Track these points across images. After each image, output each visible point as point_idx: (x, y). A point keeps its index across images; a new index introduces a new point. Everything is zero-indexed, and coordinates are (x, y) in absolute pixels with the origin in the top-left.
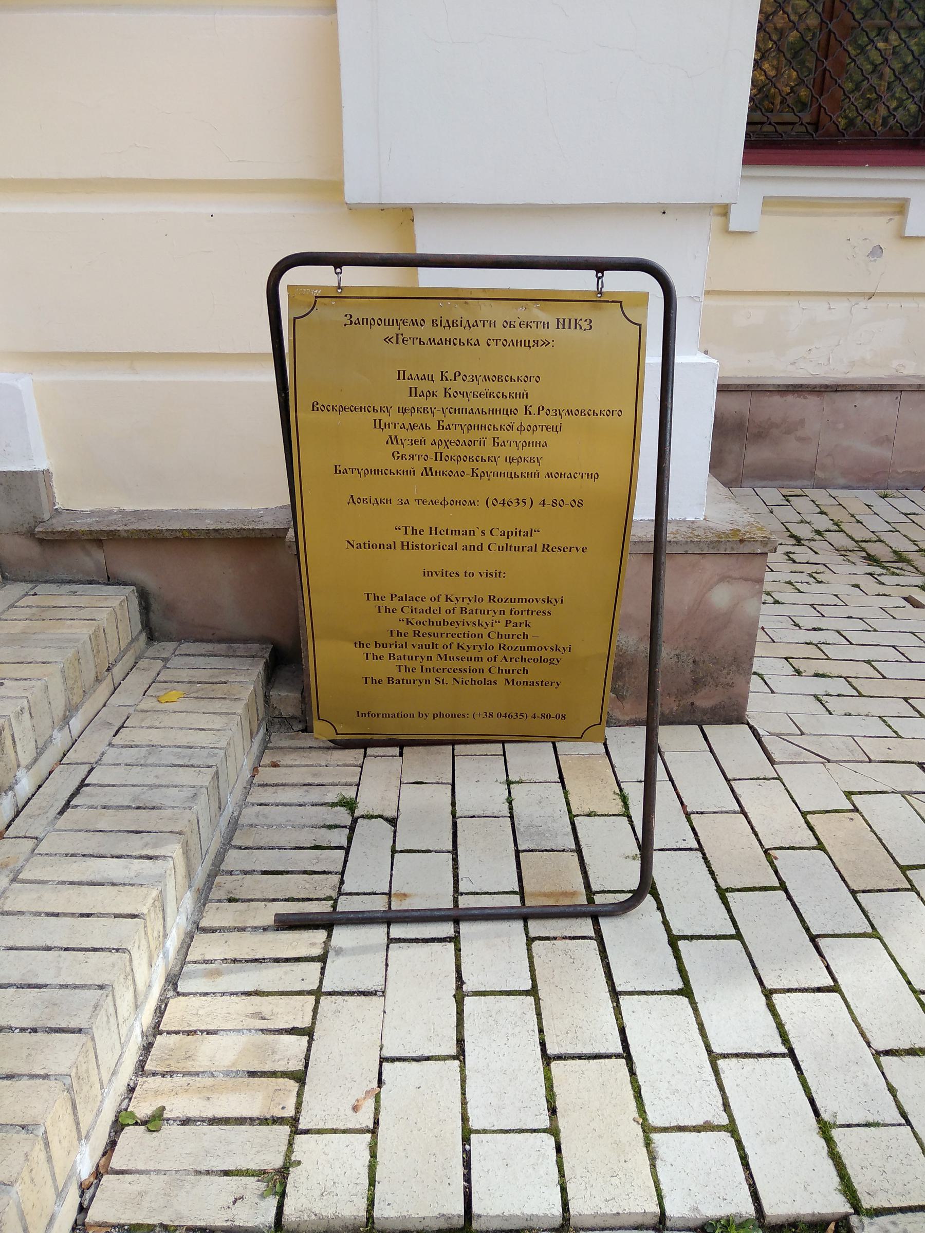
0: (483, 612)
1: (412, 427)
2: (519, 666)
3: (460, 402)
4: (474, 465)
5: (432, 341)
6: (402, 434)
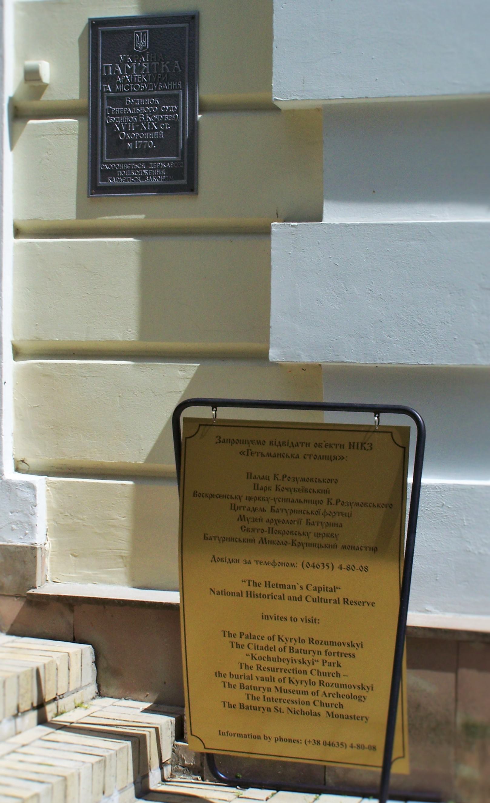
0: (305, 652)
1: (255, 510)
2: (336, 701)
3: (286, 494)
4: (294, 537)
5: (269, 455)
6: (248, 514)
